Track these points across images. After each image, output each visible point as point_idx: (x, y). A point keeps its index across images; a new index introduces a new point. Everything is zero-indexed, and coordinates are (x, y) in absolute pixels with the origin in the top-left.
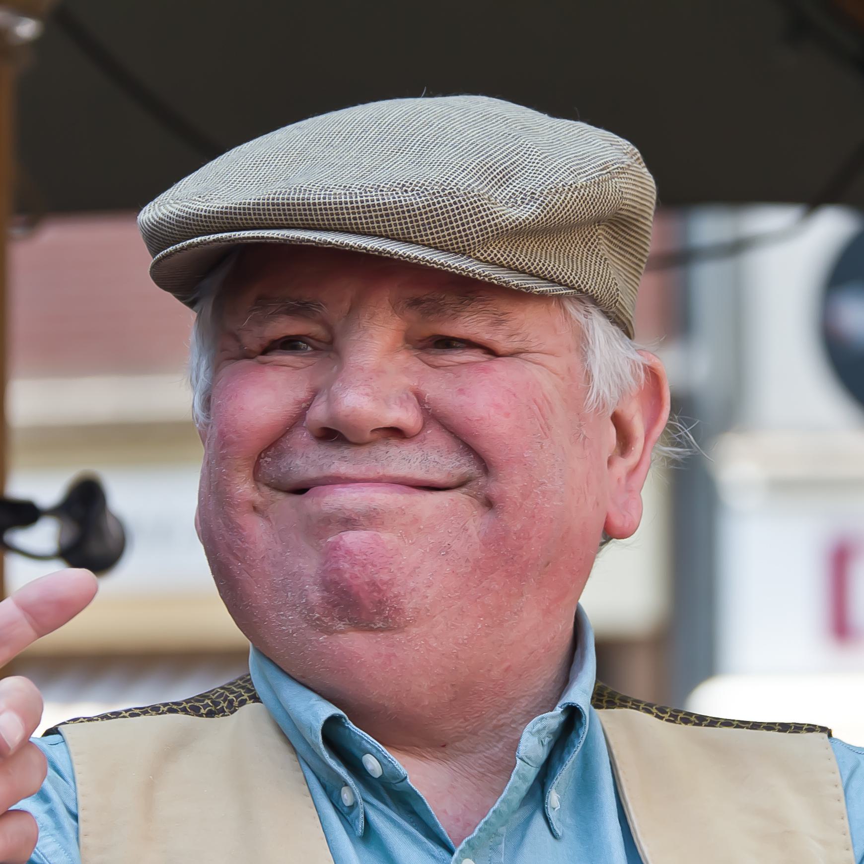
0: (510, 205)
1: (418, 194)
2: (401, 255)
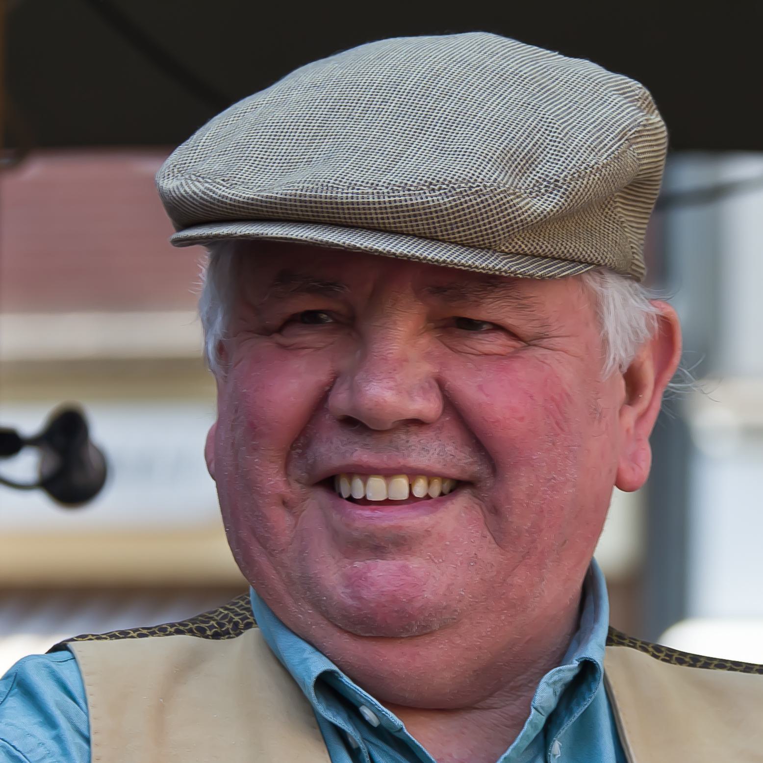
0: (534, 194)
1: (445, 193)
2: (429, 260)
